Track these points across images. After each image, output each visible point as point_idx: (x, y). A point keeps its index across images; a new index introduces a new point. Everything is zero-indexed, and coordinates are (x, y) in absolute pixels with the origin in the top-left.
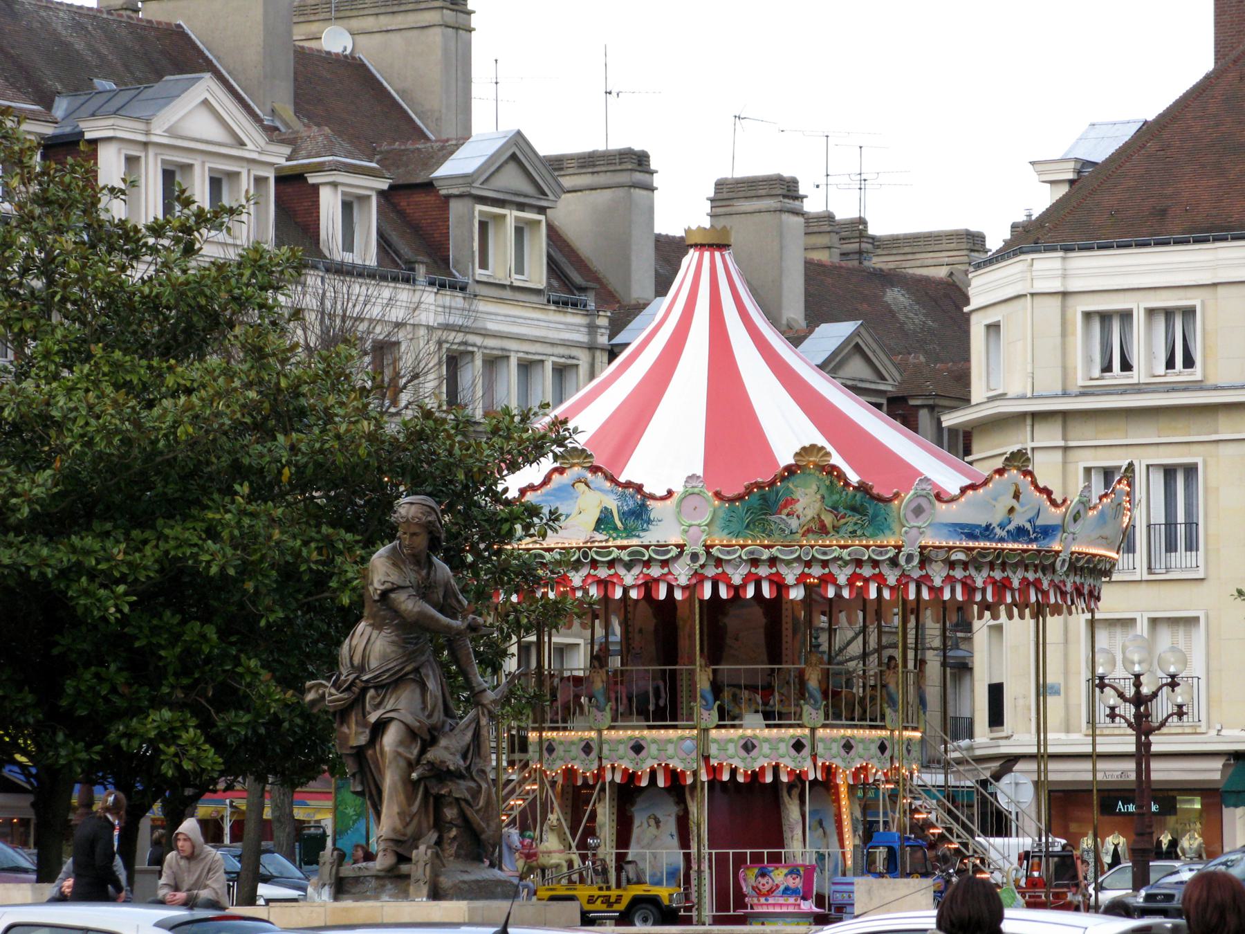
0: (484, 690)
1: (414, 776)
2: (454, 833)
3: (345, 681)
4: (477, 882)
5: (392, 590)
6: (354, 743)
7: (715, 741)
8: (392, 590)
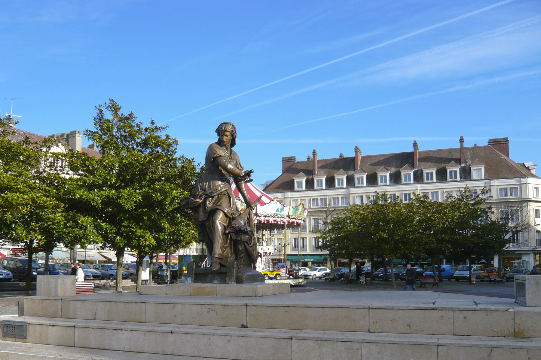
1: (227, 232)
4: (252, 275)
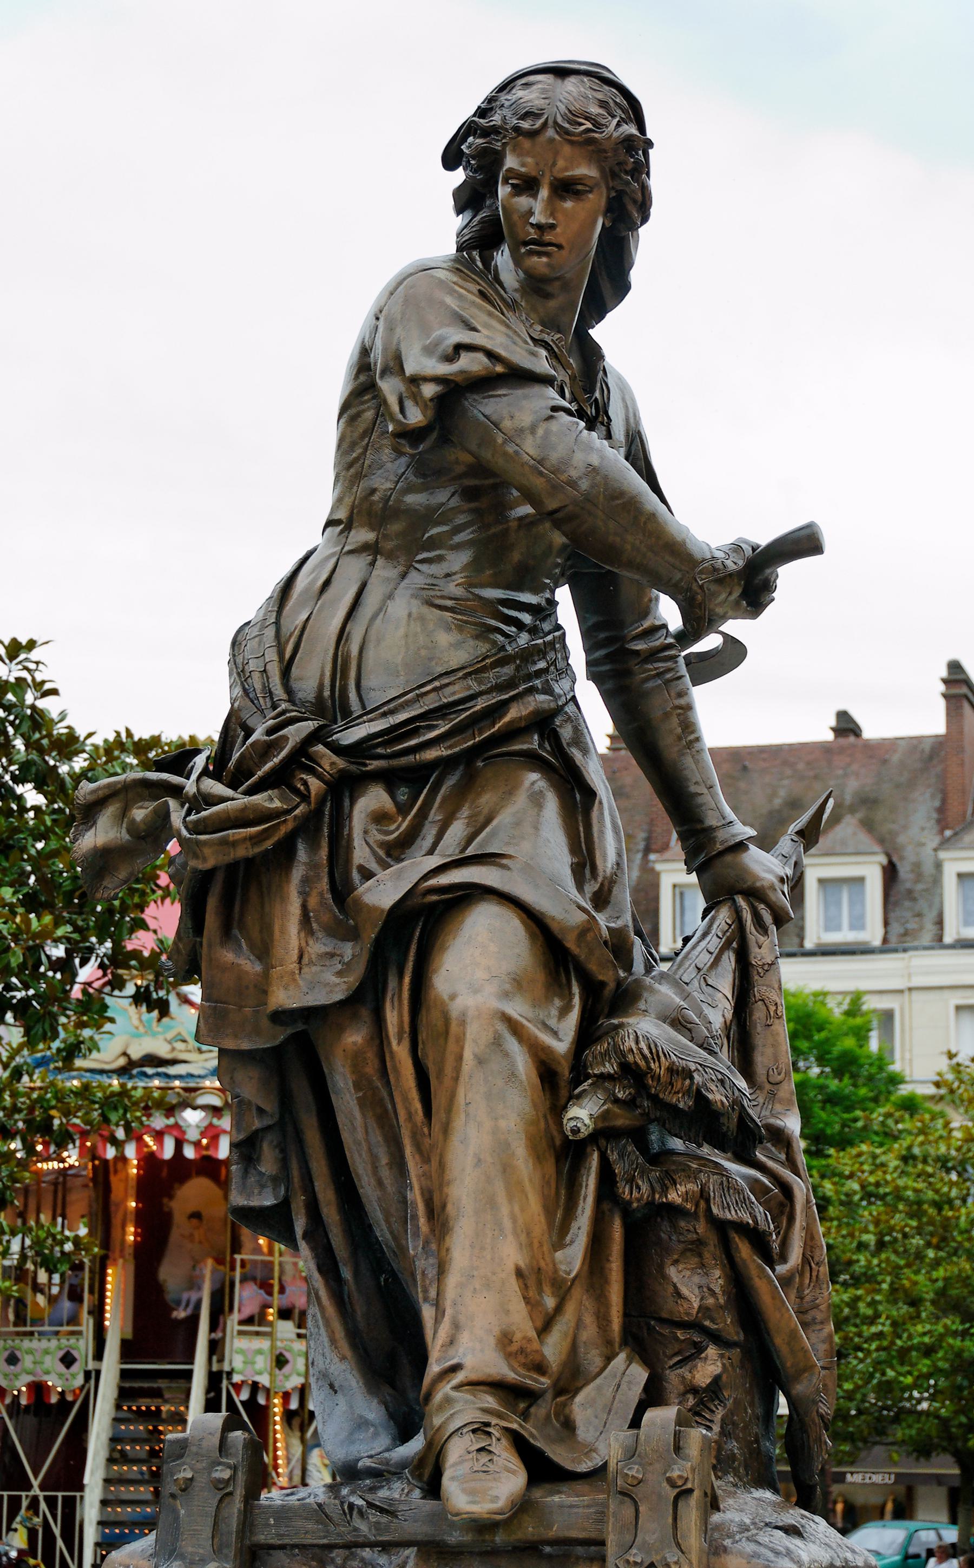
0: (740, 846)
2: (709, 1367)
3: (267, 750)
5: (483, 384)
6: (285, 997)
7: (241, 1352)
8: (483, 384)
